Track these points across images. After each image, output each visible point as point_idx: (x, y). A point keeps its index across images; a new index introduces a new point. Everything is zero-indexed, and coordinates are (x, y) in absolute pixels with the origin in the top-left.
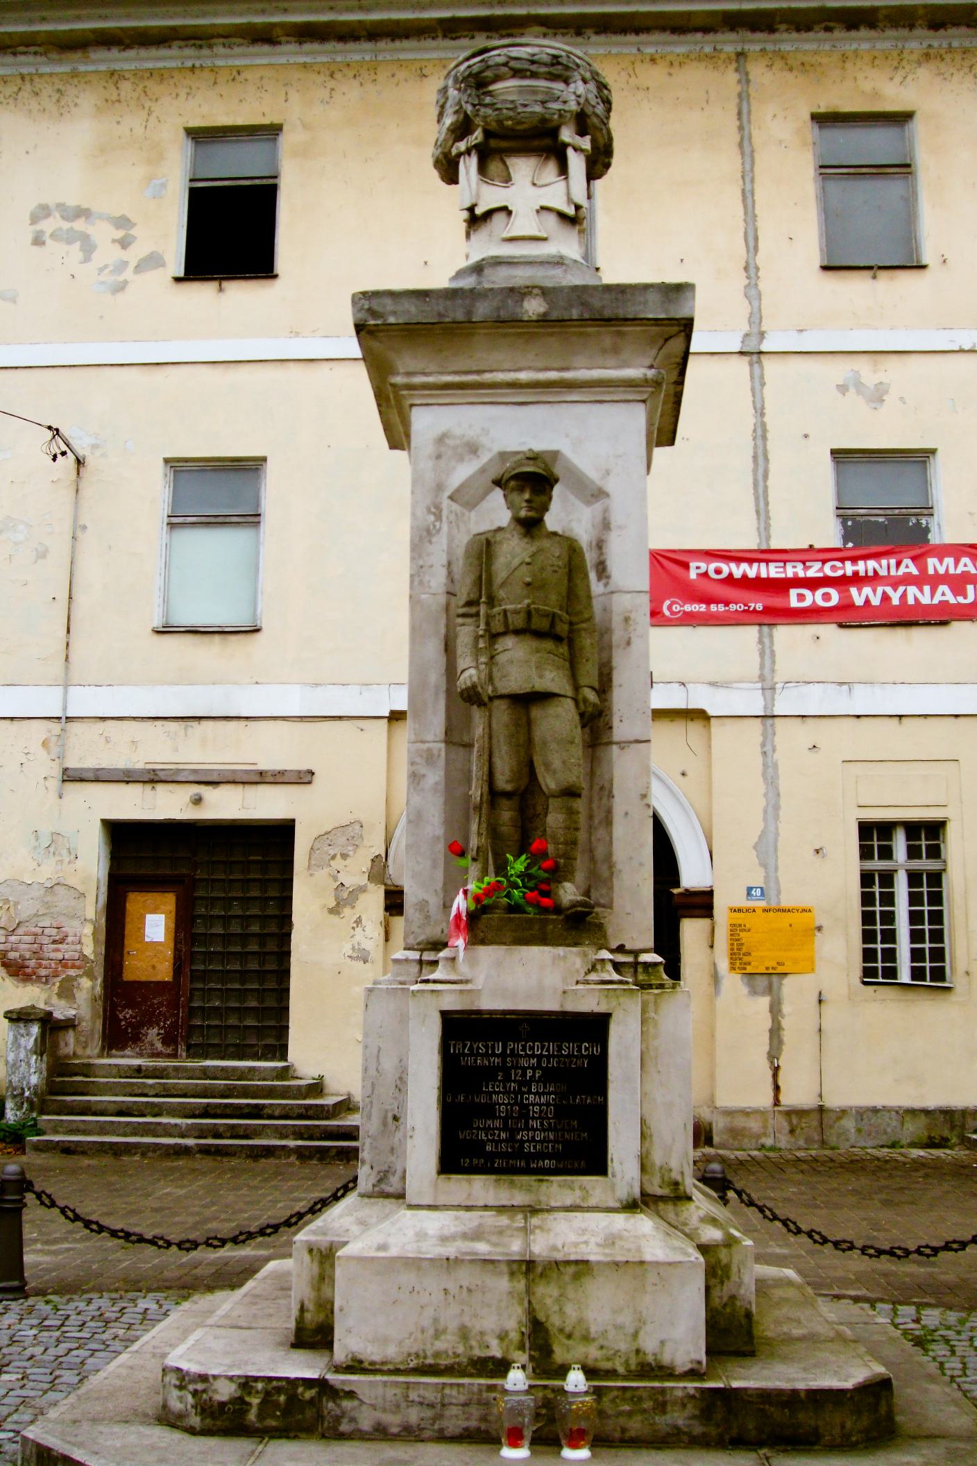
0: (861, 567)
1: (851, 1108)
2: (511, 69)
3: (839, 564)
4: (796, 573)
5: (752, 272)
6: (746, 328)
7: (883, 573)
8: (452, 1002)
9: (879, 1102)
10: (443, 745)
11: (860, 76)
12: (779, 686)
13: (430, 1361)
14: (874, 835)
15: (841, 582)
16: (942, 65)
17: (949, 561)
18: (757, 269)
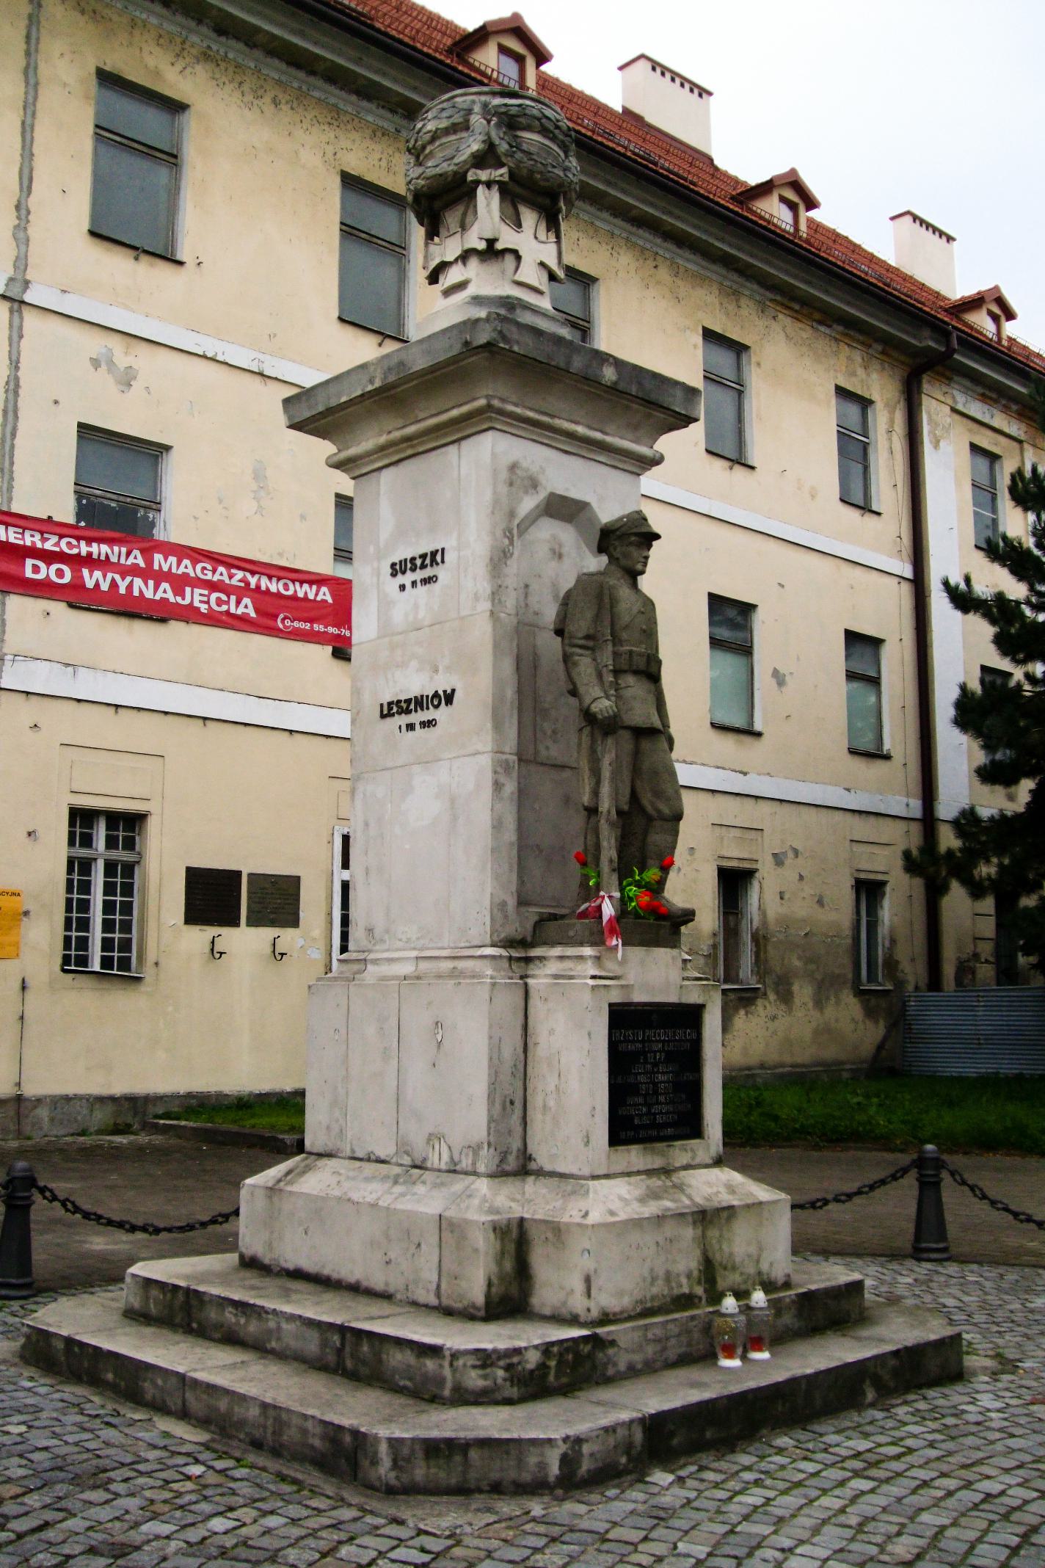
0: (94, 548)
1: (45, 1097)
2: (542, 125)
3: (74, 542)
4: (33, 543)
5: (23, 212)
6: (11, 272)
7: (114, 559)
8: (616, 997)
9: (70, 1090)
10: (515, 758)
11: (146, 49)
12: (9, 657)
13: (649, 1305)
14: (81, 819)
15: (78, 562)
16: (217, 70)
17: (173, 560)
18: (29, 212)
